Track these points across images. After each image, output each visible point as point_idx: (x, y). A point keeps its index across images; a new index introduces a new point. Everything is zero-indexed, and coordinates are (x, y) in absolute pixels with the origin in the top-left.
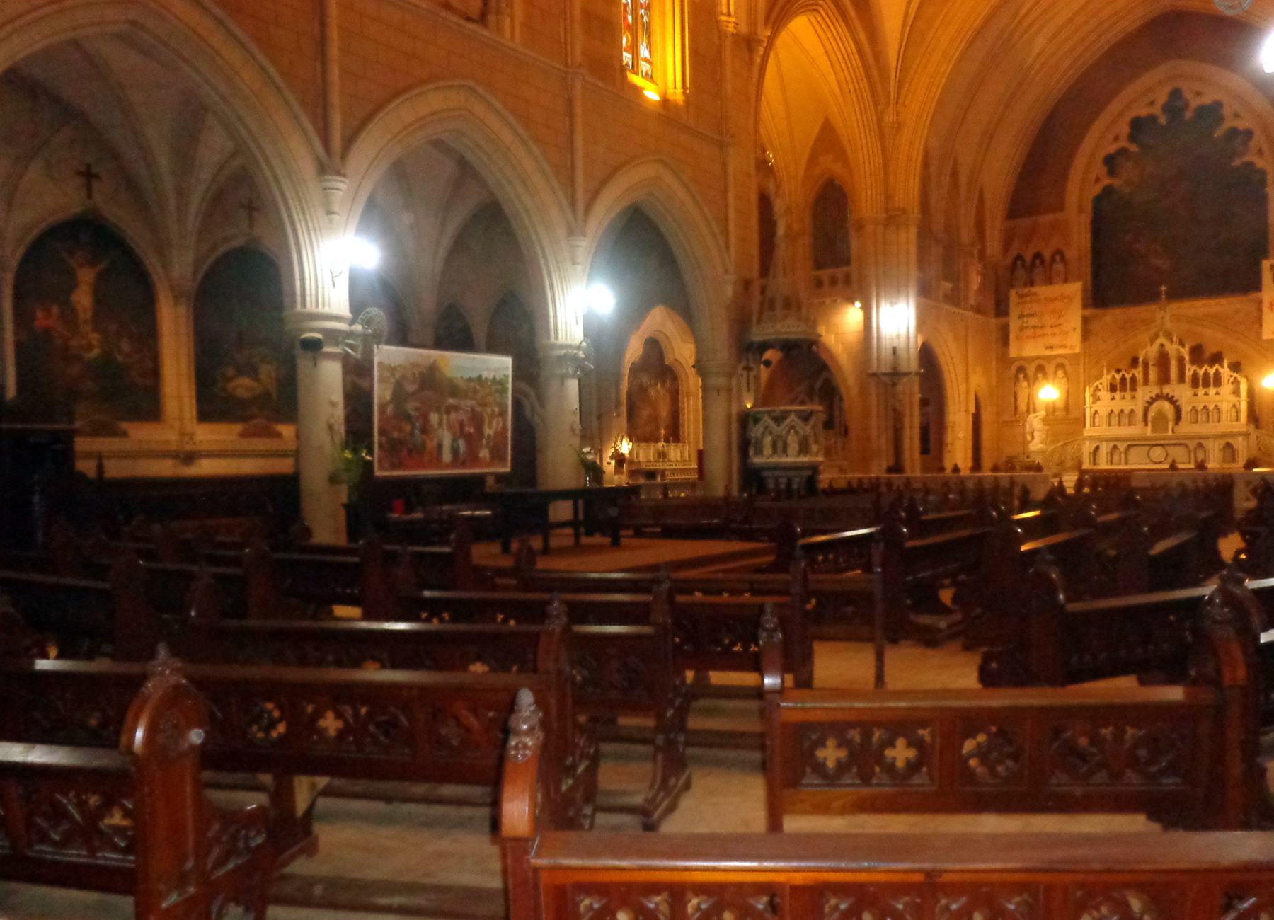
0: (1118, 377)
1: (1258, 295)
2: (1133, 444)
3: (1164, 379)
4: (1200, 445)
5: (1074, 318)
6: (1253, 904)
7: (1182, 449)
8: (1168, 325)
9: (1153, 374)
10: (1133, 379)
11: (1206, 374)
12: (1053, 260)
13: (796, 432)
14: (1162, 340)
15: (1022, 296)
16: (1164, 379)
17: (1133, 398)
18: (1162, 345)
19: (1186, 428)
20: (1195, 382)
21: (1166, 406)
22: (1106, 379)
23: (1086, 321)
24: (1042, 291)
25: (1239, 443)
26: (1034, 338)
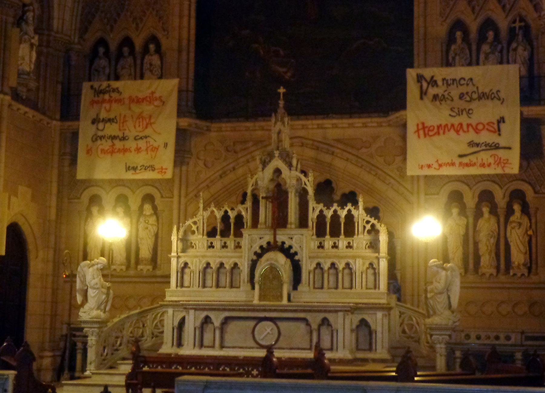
0: (219, 215)
1: (402, 113)
2: (233, 315)
3: (280, 221)
4: (325, 322)
5: (165, 129)
6: (335, 365)
7: (302, 326)
8: (287, 149)
9: (265, 212)
10: (239, 218)
11: (335, 216)
12: (146, 50)
14: (277, 163)
15: (99, 92)
16: (280, 221)
17: (238, 246)
18: (278, 171)
19: (307, 295)
20: (320, 232)
21: (281, 260)
22: (202, 216)
23: (182, 134)
24: (128, 87)
25: (377, 321)
26: (112, 152)
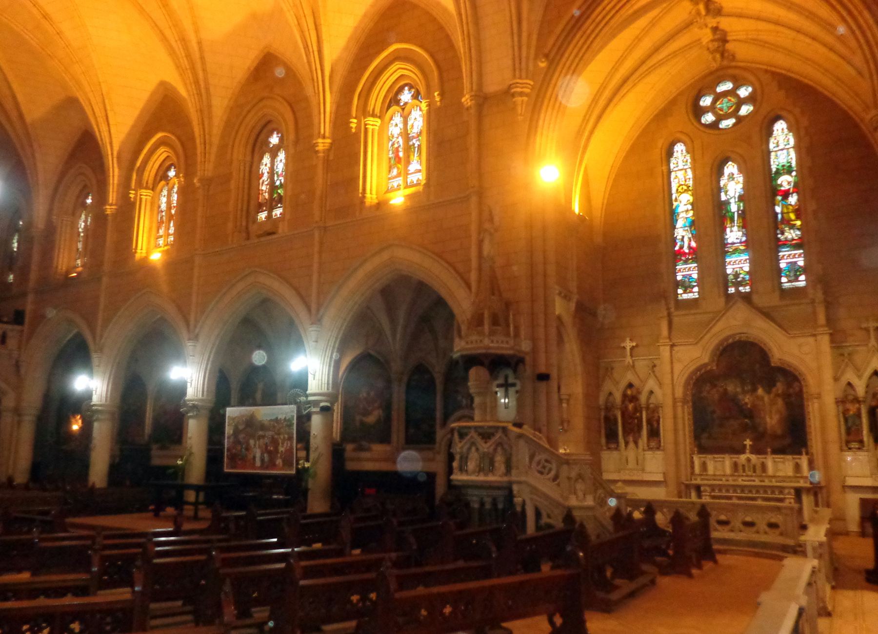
13: (477, 449)
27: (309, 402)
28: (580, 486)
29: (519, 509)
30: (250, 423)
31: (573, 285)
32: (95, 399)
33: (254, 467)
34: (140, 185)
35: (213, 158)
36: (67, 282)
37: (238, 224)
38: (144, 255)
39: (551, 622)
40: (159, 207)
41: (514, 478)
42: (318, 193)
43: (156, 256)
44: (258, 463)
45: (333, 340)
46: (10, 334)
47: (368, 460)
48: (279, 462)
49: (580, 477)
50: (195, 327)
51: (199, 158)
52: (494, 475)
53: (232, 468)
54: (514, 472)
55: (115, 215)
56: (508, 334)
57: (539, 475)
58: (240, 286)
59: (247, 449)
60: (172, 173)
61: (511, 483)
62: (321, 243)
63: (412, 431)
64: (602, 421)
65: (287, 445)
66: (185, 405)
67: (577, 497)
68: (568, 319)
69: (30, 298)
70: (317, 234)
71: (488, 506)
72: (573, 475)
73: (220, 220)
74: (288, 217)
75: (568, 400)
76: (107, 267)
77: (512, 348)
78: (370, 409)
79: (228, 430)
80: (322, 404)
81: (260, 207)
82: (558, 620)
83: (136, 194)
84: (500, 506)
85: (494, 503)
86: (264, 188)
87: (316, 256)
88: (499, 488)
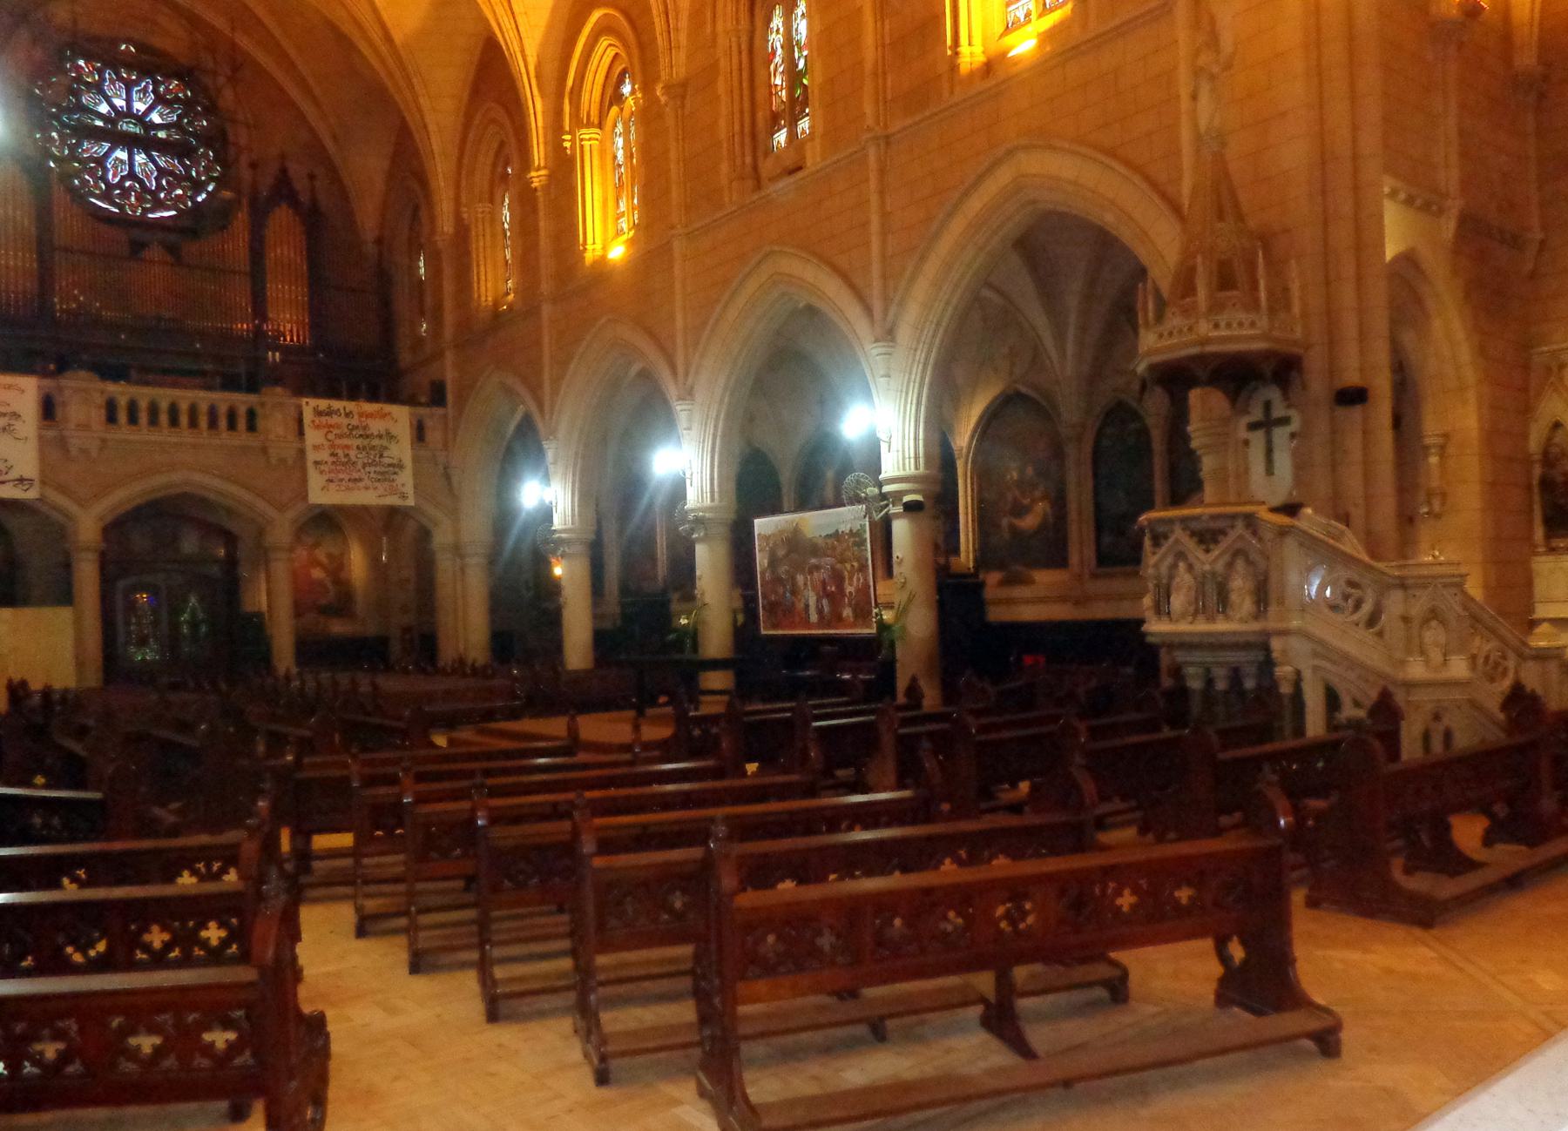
13: (1190, 568)
27: (884, 496)
28: (1433, 635)
29: (1286, 689)
30: (794, 543)
31: (1450, 177)
32: (558, 523)
33: (807, 624)
34: (578, 122)
35: (683, 38)
36: (497, 318)
37: (739, 162)
38: (599, 253)
39: (1224, 958)
40: (615, 157)
41: (1272, 624)
42: (868, 66)
43: (618, 252)
44: (814, 617)
45: (917, 370)
46: (429, 423)
47: (1028, 601)
48: (847, 612)
49: (1434, 614)
50: (687, 374)
51: (661, 42)
52: (1228, 618)
53: (775, 627)
54: (1273, 609)
55: (546, 188)
56: (1254, 305)
57: (1331, 614)
58: (752, 286)
59: (794, 592)
60: (626, 89)
61: (1267, 634)
62: (882, 172)
63: (1107, 539)
64: (1536, 490)
65: (857, 580)
66: (684, 520)
67: (1427, 662)
68: (1437, 266)
69: (449, 357)
70: (872, 153)
71: (1221, 685)
72: (1417, 609)
73: (714, 167)
74: (820, 130)
75: (1443, 447)
76: (546, 287)
77: (1265, 337)
78: (1026, 501)
79: (761, 560)
80: (906, 499)
81: (774, 123)
82: (1237, 952)
83: (573, 141)
84: (1249, 684)
85: (1236, 675)
86: (778, 81)
87: (874, 199)
88: (1236, 646)
